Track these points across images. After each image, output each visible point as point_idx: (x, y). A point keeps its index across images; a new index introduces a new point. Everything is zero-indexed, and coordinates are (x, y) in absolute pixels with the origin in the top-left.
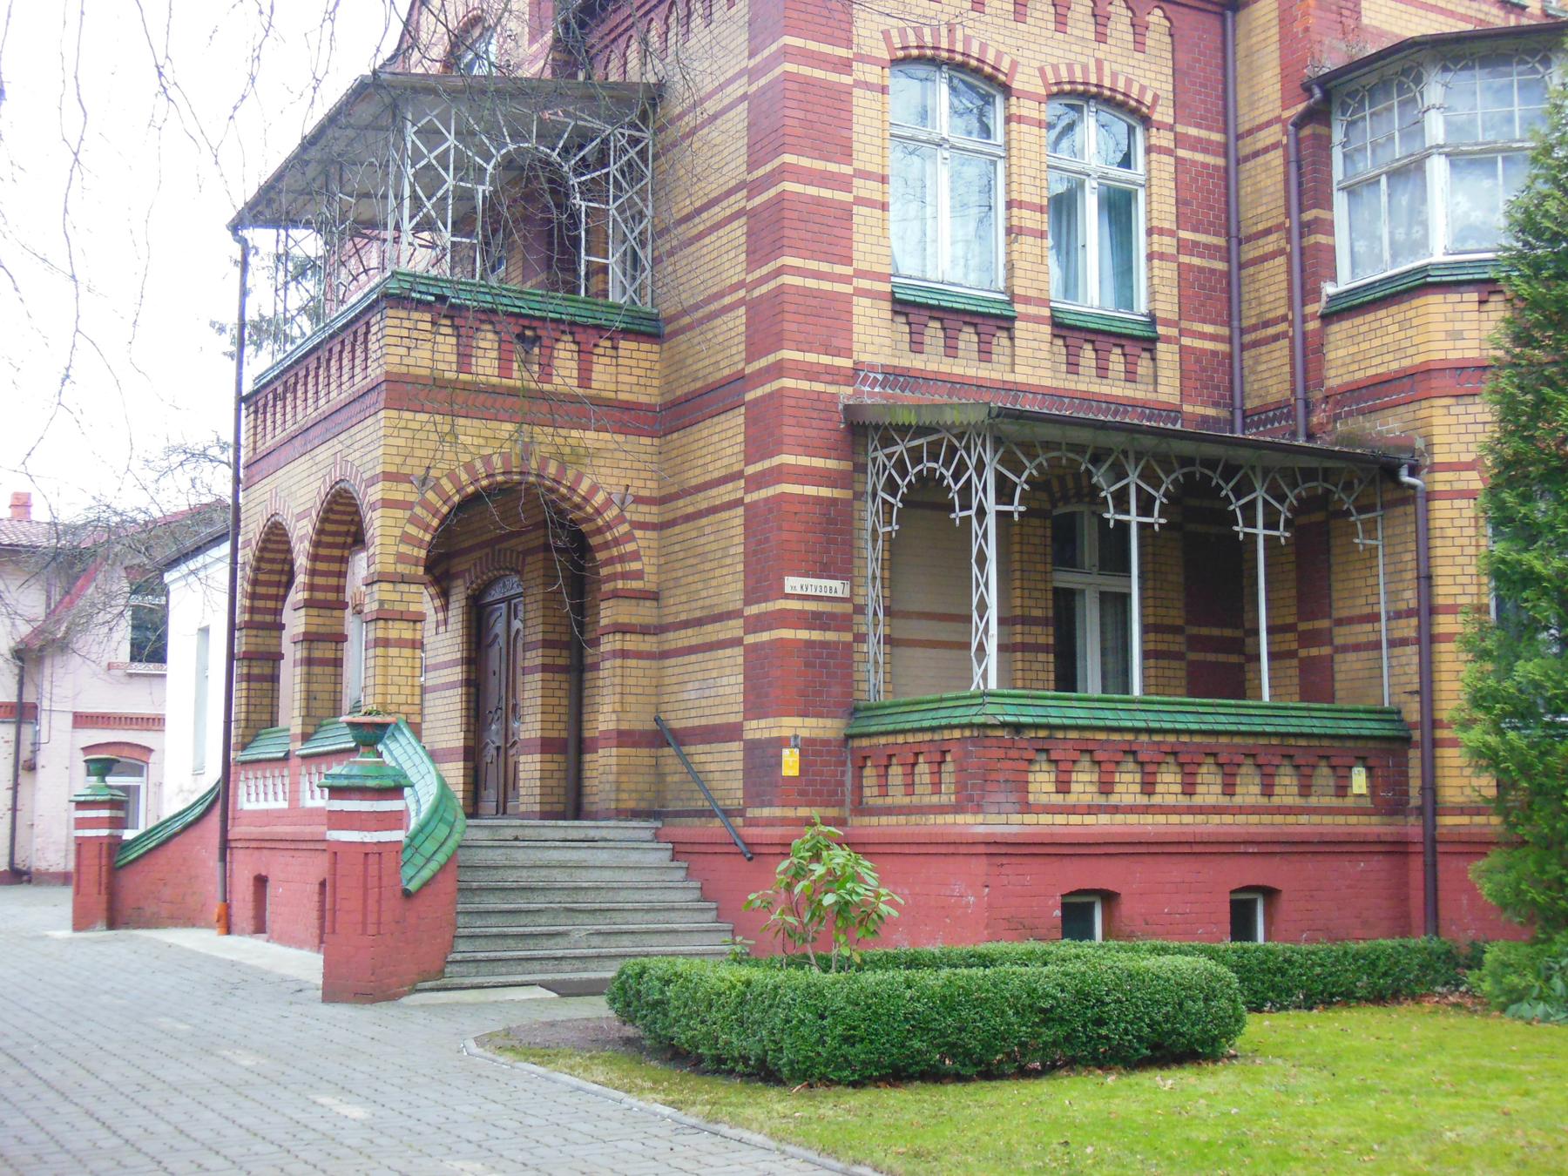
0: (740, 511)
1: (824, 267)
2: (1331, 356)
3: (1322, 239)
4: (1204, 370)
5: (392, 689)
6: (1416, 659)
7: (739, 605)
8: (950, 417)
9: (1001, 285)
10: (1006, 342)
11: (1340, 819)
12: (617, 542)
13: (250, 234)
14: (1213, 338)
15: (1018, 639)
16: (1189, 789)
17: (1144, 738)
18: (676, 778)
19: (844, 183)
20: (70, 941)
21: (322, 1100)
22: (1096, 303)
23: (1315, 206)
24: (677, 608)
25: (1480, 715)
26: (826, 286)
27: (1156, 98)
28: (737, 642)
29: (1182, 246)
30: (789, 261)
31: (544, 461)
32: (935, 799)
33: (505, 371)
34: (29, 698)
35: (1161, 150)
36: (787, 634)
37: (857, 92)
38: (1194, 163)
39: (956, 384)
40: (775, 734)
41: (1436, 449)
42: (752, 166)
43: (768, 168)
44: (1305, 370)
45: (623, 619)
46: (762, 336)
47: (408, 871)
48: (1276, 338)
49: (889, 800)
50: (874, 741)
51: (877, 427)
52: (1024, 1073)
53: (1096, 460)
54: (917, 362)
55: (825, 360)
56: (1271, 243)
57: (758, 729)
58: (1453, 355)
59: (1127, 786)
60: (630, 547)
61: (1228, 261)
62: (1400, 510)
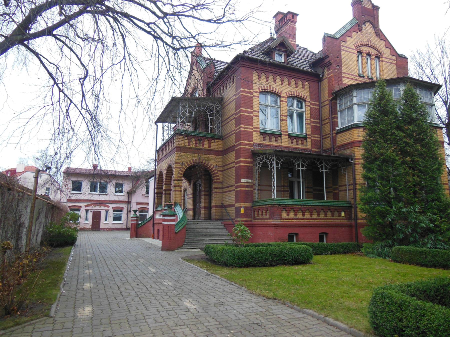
0: (234, 168)
2: (337, 140)
3: (336, 120)
4: (315, 143)
5: (177, 198)
6: (353, 193)
7: (234, 184)
8: (268, 152)
9: (279, 129)
10: (280, 139)
11: (339, 221)
12: (215, 174)
13: (158, 124)
14: (317, 137)
15: (283, 189)
16: (311, 215)
17: (303, 206)
18: (225, 213)
19: (251, 113)
20: (129, 240)
21: (150, 268)
24: (225, 185)
25: (362, 203)
26: (248, 130)
27: (307, 97)
28: (234, 190)
29: (311, 122)
30: (241, 126)
31: (203, 160)
32: (266, 217)
34: (130, 200)
35: (308, 106)
36: (242, 189)
37: (253, 97)
38: (314, 108)
39: (271, 146)
40: (240, 206)
41: (356, 156)
42: (236, 110)
43: (239, 110)
44: (333, 143)
45: (216, 187)
46: (238, 138)
47: (176, 229)
48: (328, 137)
49: (259, 217)
50: (256, 207)
51: (257, 154)
52: (272, 266)
53: (318, 161)
54: (264, 143)
56: (327, 121)
57: (237, 205)
59: (300, 215)
60: (217, 174)
61: (320, 124)
62: (350, 166)
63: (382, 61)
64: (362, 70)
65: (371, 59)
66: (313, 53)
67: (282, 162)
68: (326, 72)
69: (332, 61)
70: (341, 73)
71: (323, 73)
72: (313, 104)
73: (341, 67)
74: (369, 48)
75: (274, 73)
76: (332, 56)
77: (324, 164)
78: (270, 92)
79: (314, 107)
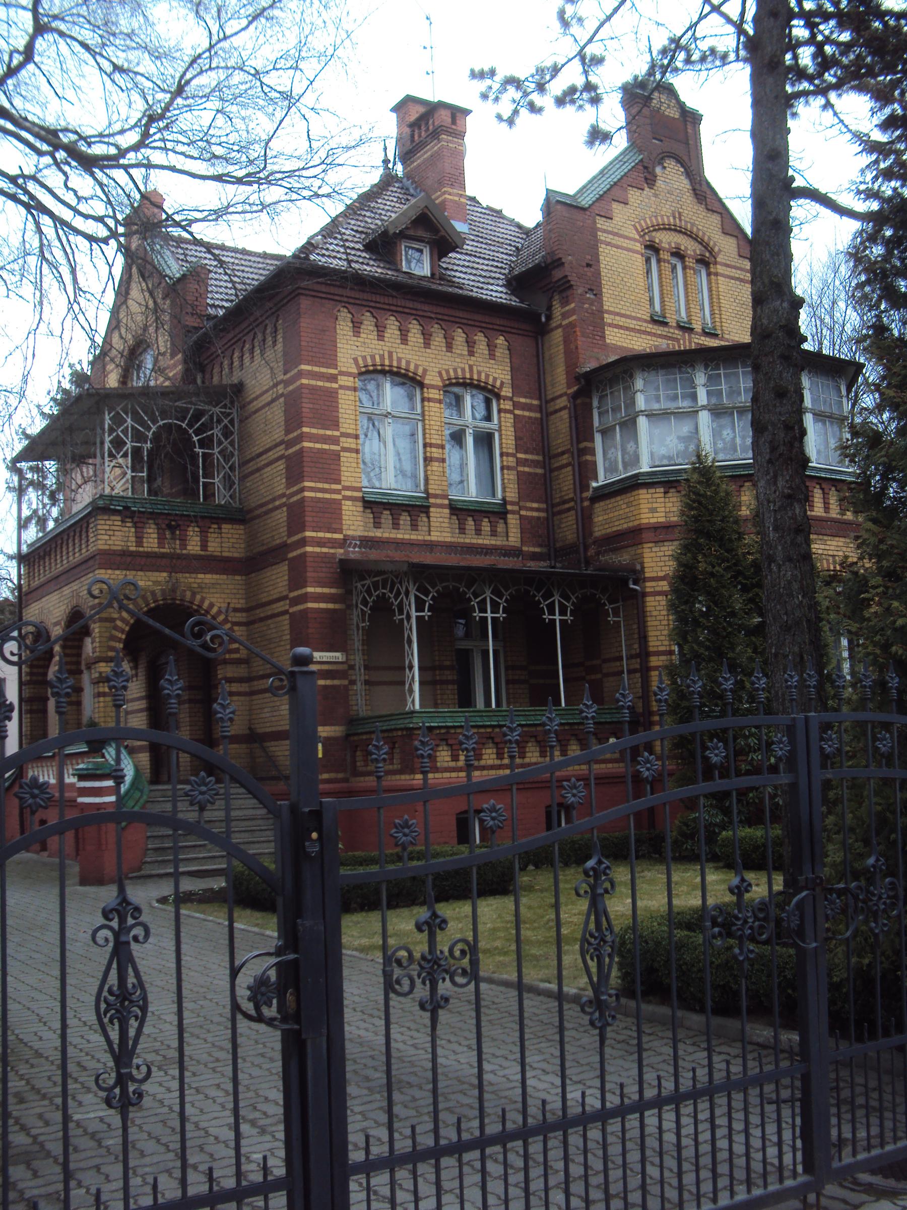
0: (287, 617)
1: (326, 486)
2: (596, 520)
3: (589, 458)
10: (425, 519)
14: (537, 510)
17: (497, 730)
19: (335, 441)
22: (474, 495)
23: (585, 440)
26: (327, 496)
27: (502, 383)
29: (519, 462)
30: (307, 484)
33: (161, 544)
35: (506, 411)
37: (340, 391)
38: (524, 416)
43: (295, 434)
48: (569, 510)
54: (378, 533)
55: (329, 535)
56: (565, 459)
58: (653, 521)
63: (716, 274)
64: (662, 301)
65: (684, 268)
66: (519, 226)
67: (433, 598)
68: (557, 311)
69: (574, 279)
70: (601, 312)
71: (550, 308)
72: (524, 407)
73: (598, 295)
74: (681, 236)
75: (402, 313)
76: (571, 268)
77: (557, 598)
78: (391, 373)
79: (527, 414)
